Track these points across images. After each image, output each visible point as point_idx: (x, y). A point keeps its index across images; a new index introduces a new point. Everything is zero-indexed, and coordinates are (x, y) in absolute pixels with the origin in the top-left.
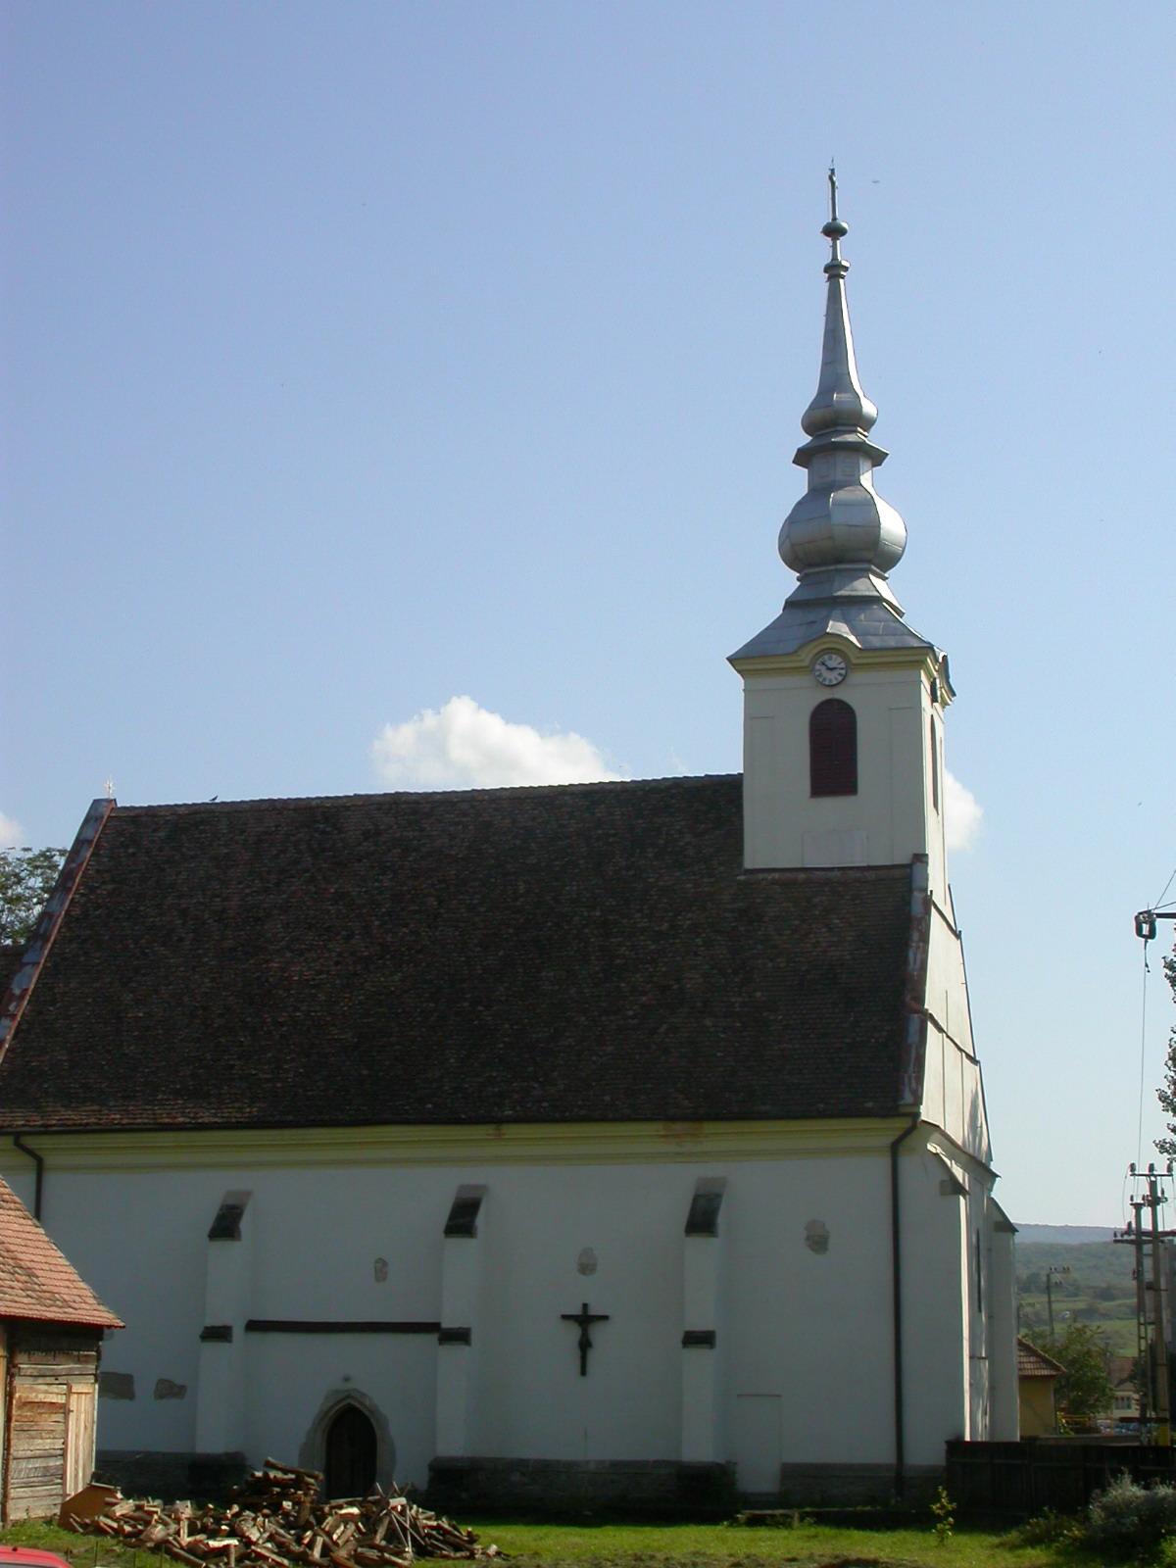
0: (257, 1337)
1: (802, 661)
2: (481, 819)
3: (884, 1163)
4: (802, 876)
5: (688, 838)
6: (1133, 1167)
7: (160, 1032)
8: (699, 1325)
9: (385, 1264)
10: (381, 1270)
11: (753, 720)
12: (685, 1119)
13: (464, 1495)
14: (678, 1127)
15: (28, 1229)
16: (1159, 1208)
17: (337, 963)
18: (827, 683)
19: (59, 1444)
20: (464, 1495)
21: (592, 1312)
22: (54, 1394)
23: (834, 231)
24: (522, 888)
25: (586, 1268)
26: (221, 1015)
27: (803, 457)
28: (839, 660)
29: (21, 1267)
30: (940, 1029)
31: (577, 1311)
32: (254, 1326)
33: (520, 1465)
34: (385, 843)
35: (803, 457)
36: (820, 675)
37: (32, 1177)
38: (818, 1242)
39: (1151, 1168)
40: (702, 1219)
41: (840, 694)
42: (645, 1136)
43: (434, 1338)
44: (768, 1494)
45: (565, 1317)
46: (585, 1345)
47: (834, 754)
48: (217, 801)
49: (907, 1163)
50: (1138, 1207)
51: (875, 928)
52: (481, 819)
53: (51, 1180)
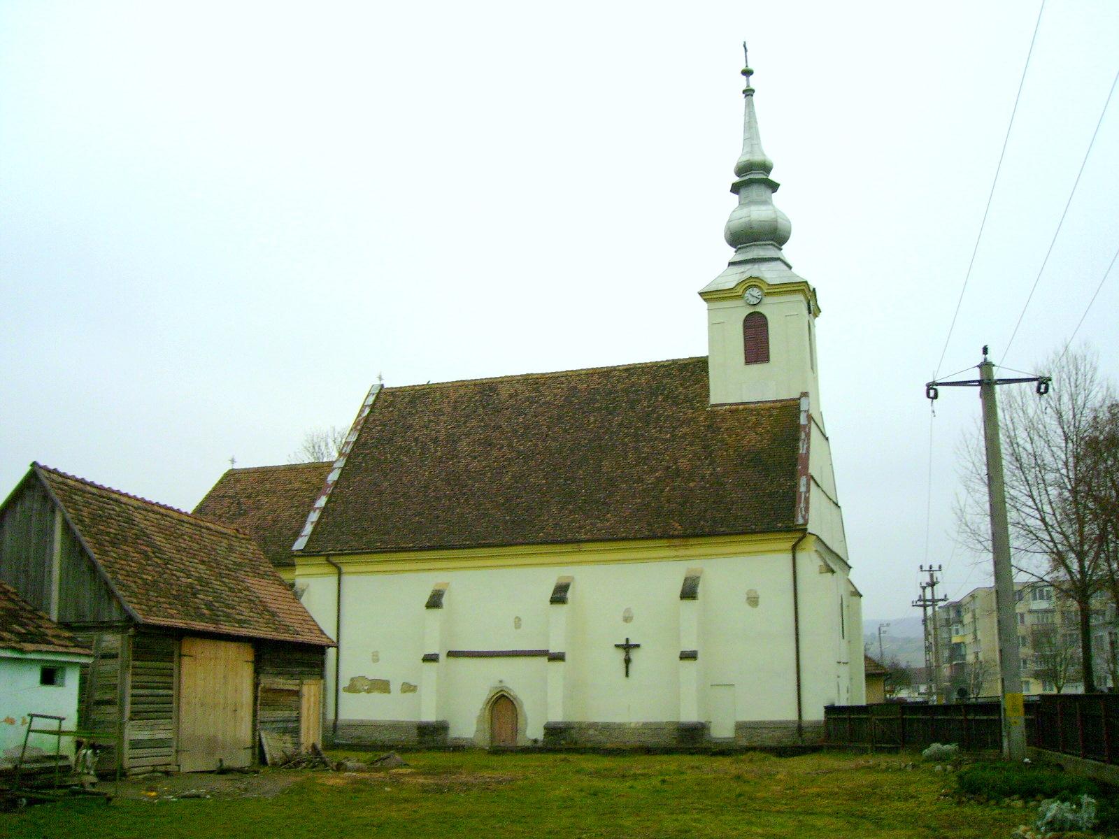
0: (452, 660)
1: (738, 292)
2: (571, 385)
3: (790, 556)
4: (741, 407)
5: (681, 389)
6: (921, 567)
7: (402, 500)
8: (689, 647)
9: (520, 619)
10: (518, 622)
12: (678, 537)
13: (563, 742)
14: (677, 542)
15: (280, 590)
16: (935, 587)
17: (494, 462)
18: (752, 303)
19: (295, 714)
20: (563, 742)
21: (632, 642)
22: (290, 685)
23: (747, 73)
24: (592, 419)
25: (627, 619)
26: (434, 491)
28: (758, 290)
29: (268, 611)
30: (818, 486)
31: (623, 642)
32: (452, 654)
33: (593, 725)
34: (520, 400)
36: (748, 299)
37: (336, 578)
38: (753, 601)
39: (931, 567)
40: (689, 592)
41: (758, 309)
42: (660, 550)
43: (545, 659)
44: (728, 738)
45: (617, 646)
46: (628, 661)
47: (756, 344)
48: (430, 383)
50: (924, 588)
52: (571, 385)
53: (345, 578)
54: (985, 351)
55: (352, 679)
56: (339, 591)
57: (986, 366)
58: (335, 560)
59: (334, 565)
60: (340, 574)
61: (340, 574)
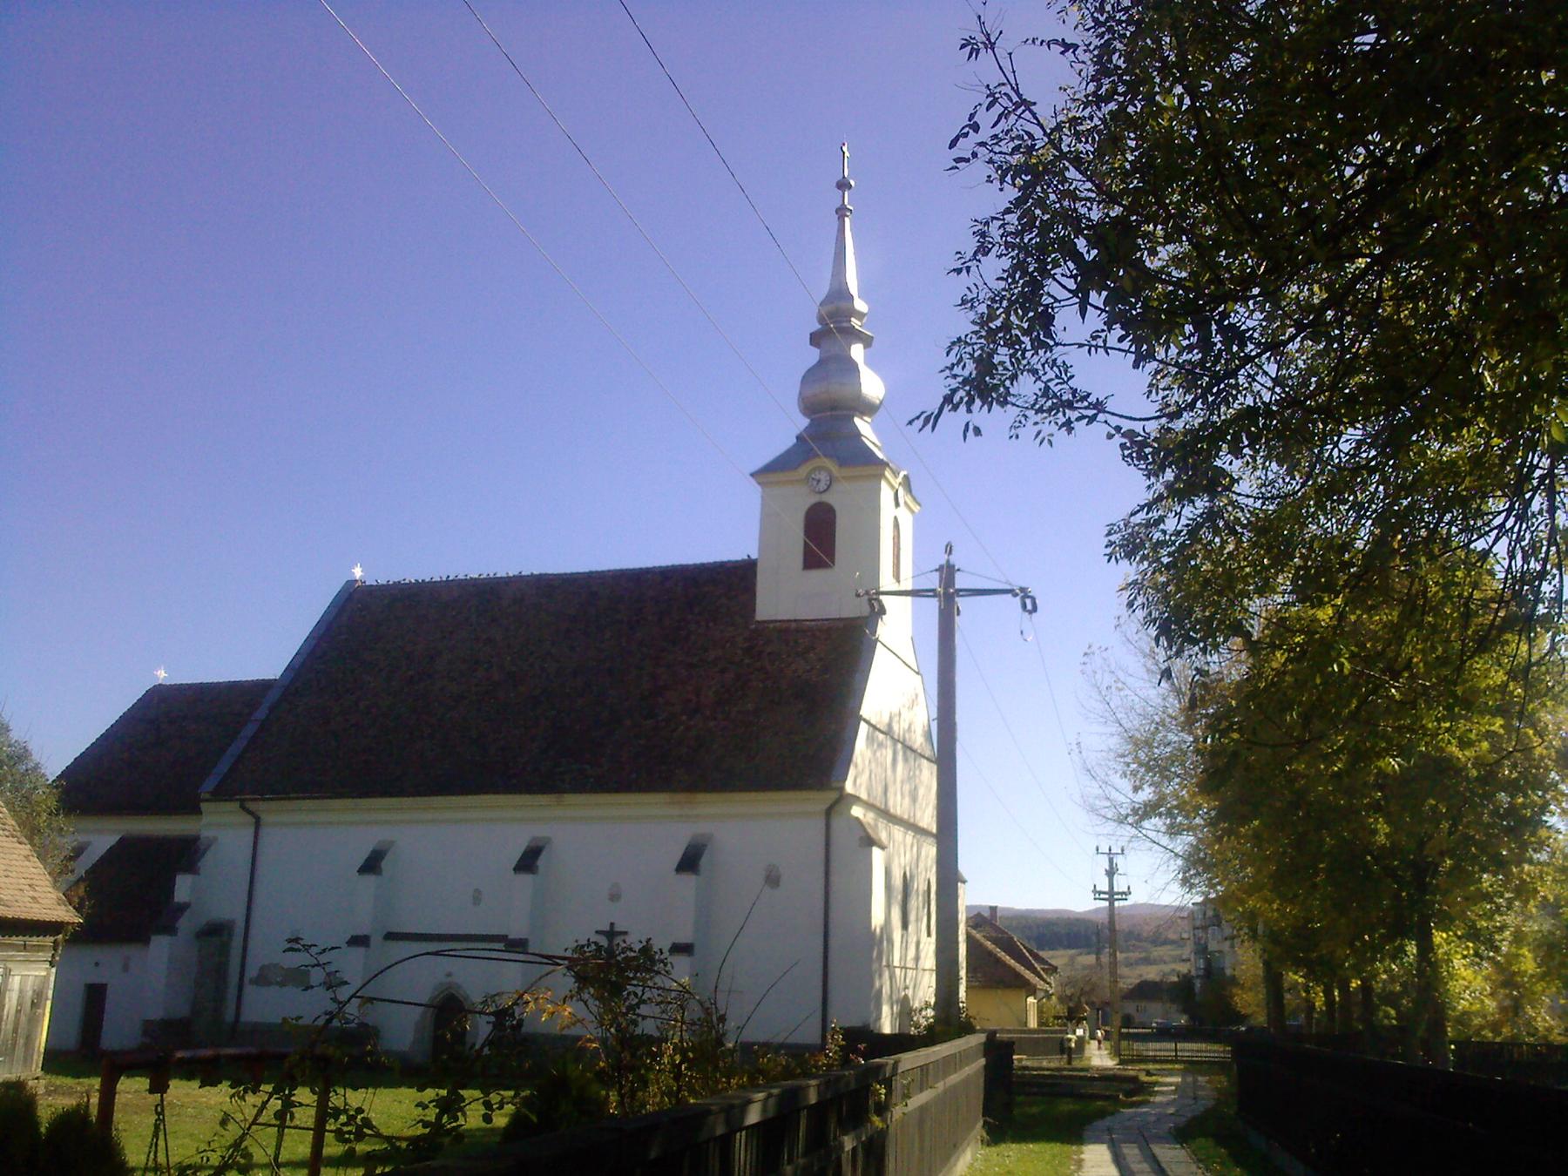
3: (821, 824)
10: (477, 898)
11: (767, 519)
21: (617, 929)
23: (843, 185)
25: (615, 897)
27: (815, 339)
31: (607, 928)
32: (391, 936)
35: (815, 339)
37: (252, 830)
41: (826, 498)
47: (820, 538)
49: (837, 823)
51: (833, 657)
54: (949, 549)
55: (262, 968)
56: (255, 844)
57: (948, 572)
58: (251, 806)
59: (251, 813)
60: (258, 824)
61: (258, 824)
